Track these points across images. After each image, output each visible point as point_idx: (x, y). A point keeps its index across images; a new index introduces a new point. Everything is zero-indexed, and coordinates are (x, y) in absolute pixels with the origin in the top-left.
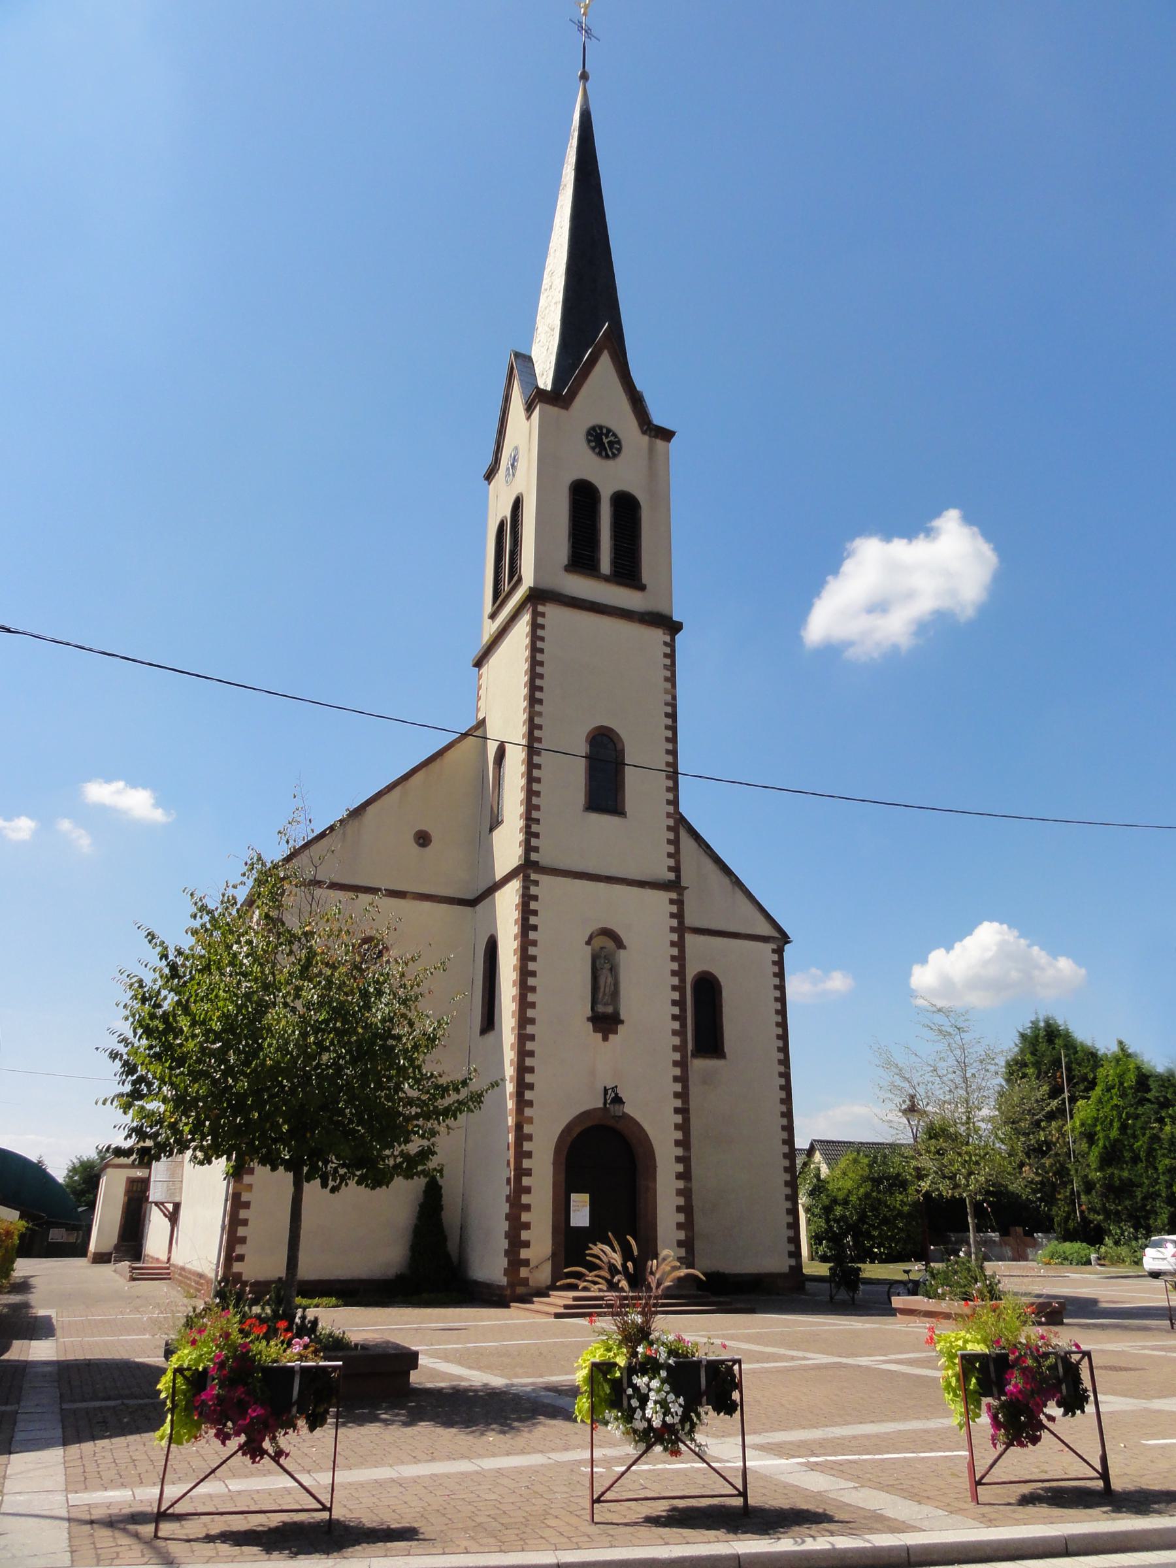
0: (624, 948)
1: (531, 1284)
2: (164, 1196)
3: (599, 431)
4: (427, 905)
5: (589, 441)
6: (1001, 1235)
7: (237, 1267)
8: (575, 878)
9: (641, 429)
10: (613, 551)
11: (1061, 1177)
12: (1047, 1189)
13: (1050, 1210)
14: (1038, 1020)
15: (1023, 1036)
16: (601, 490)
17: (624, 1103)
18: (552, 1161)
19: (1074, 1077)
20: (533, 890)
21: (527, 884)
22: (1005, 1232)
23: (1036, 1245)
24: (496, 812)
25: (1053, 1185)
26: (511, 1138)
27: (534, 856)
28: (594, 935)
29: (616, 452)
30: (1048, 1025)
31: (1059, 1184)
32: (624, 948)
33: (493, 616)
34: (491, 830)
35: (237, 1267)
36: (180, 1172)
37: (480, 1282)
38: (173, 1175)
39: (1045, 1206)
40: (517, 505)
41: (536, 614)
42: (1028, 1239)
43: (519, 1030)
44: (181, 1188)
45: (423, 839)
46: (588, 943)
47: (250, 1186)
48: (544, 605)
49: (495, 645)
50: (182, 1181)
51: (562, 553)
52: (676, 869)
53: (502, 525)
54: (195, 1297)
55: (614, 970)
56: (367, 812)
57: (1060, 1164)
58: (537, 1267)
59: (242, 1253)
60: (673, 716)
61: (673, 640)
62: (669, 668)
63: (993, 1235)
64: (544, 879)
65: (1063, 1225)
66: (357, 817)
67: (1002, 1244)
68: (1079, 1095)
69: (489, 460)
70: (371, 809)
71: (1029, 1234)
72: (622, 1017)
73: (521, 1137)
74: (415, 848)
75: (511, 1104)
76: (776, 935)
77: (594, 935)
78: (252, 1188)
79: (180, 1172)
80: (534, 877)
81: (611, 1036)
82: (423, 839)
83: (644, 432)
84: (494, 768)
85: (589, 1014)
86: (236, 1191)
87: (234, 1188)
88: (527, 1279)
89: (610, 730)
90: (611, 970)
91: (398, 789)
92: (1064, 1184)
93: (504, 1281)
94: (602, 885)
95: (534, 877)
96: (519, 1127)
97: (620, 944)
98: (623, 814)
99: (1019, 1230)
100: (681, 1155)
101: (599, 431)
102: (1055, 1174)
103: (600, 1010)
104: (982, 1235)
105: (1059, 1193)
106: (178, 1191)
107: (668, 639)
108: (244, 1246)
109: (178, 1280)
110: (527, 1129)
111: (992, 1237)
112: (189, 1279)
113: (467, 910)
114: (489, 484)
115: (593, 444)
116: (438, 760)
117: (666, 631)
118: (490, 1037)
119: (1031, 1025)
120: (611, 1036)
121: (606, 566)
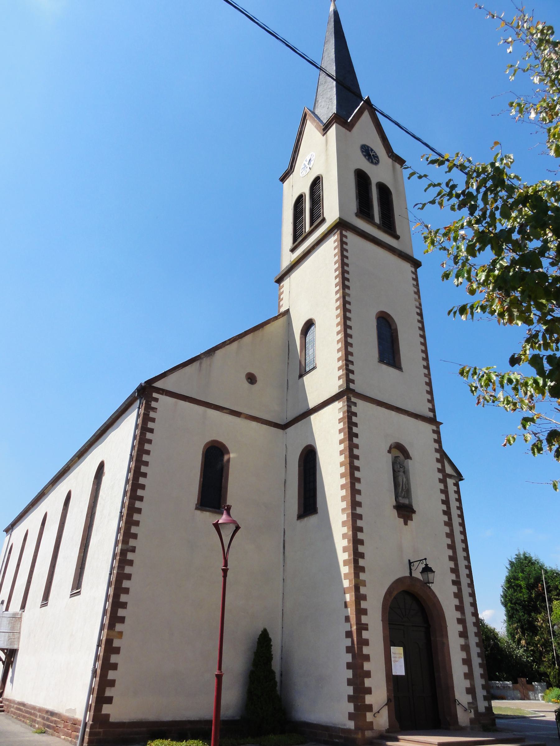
0: (411, 458)
1: (375, 728)
2: (6, 643)
3: (367, 148)
4: (254, 424)
5: (362, 152)
6: (513, 683)
7: (106, 709)
8: (378, 405)
9: (388, 155)
10: (380, 212)
11: (546, 647)
12: (537, 655)
13: (539, 667)
14: (520, 554)
15: (512, 564)
16: (372, 179)
17: (434, 572)
18: (381, 618)
19: (550, 586)
20: (354, 409)
21: (350, 404)
22: (515, 682)
23: (534, 690)
24: (304, 365)
25: (541, 653)
26: (349, 597)
27: (352, 386)
28: (392, 447)
29: (377, 162)
30: (526, 558)
31: (545, 652)
32: (411, 458)
33: (293, 250)
34: (301, 376)
35: (106, 709)
36: (19, 626)
37: (315, 724)
38: (13, 628)
39: (536, 665)
40: (317, 183)
41: (342, 236)
42: (529, 686)
43: (352, 510)
44: (19, 638)
45: (251, 379)
46: (389, 452)
47: (121, 634)
48: (346, 231)
49: (298, 264)
50: (20, 633)
51: (353, 206)
52: (433, 410)
53: (300, 200)
54: (44, 733)
55: (406, 472)
56: (215, 354)
57: (544, 639)
58: (378, 712)
59: (111, 695)
60: (421, 314)
61: (416, 271)
62: (416, 286)
63: (508, 683)
64: (359, 402)
65: (557, 677)
66: (209, 356)
67: (514, 689)
68: (554, 598)
69: (286, 167)
70: (219, 353)
71: (529, 682)
72: (415, 507)
73: (359, 598)
74: (246, 384)
75: (345, 570)
76: (454, 474)
77: (392, 447)
78: (122, 636)
79: (19, 626)
80: (353, 399)
81: (409, 522)
82: (251, 379)
83: (389, 157)
84: (301, 338)
85: (394, 503)
86: (109, 637)
87: (108, 635)
88: (372, 723)
89: (389, 315)
90: (404, 472)
91: (235, 344)
92: (548, 652)
93: (351, 725)
94: (393, 413)
95: (353, 399)
96: (357, 588)
97: (407, 456)
98: (401, 369)
99: (524, 680)
100: (460, 617)
101: (367, 148)
102: (541, 646)
103: (401, 501)
104: (501, 682)
105: (545, 657)
106: (16, 640)
107: (413, 270)
108: (113, 688)
109: (15, 713)
110: (363, 590)
111: (507, 684)
112: (34, 715)
113: (280, 431)
114: (283, 183)
115: (364, 153)
116: (261, 330)
117: (413, 266)
118: (312, 520)
119: (516, 557)
120: (409, 522)
121: (377, 219)
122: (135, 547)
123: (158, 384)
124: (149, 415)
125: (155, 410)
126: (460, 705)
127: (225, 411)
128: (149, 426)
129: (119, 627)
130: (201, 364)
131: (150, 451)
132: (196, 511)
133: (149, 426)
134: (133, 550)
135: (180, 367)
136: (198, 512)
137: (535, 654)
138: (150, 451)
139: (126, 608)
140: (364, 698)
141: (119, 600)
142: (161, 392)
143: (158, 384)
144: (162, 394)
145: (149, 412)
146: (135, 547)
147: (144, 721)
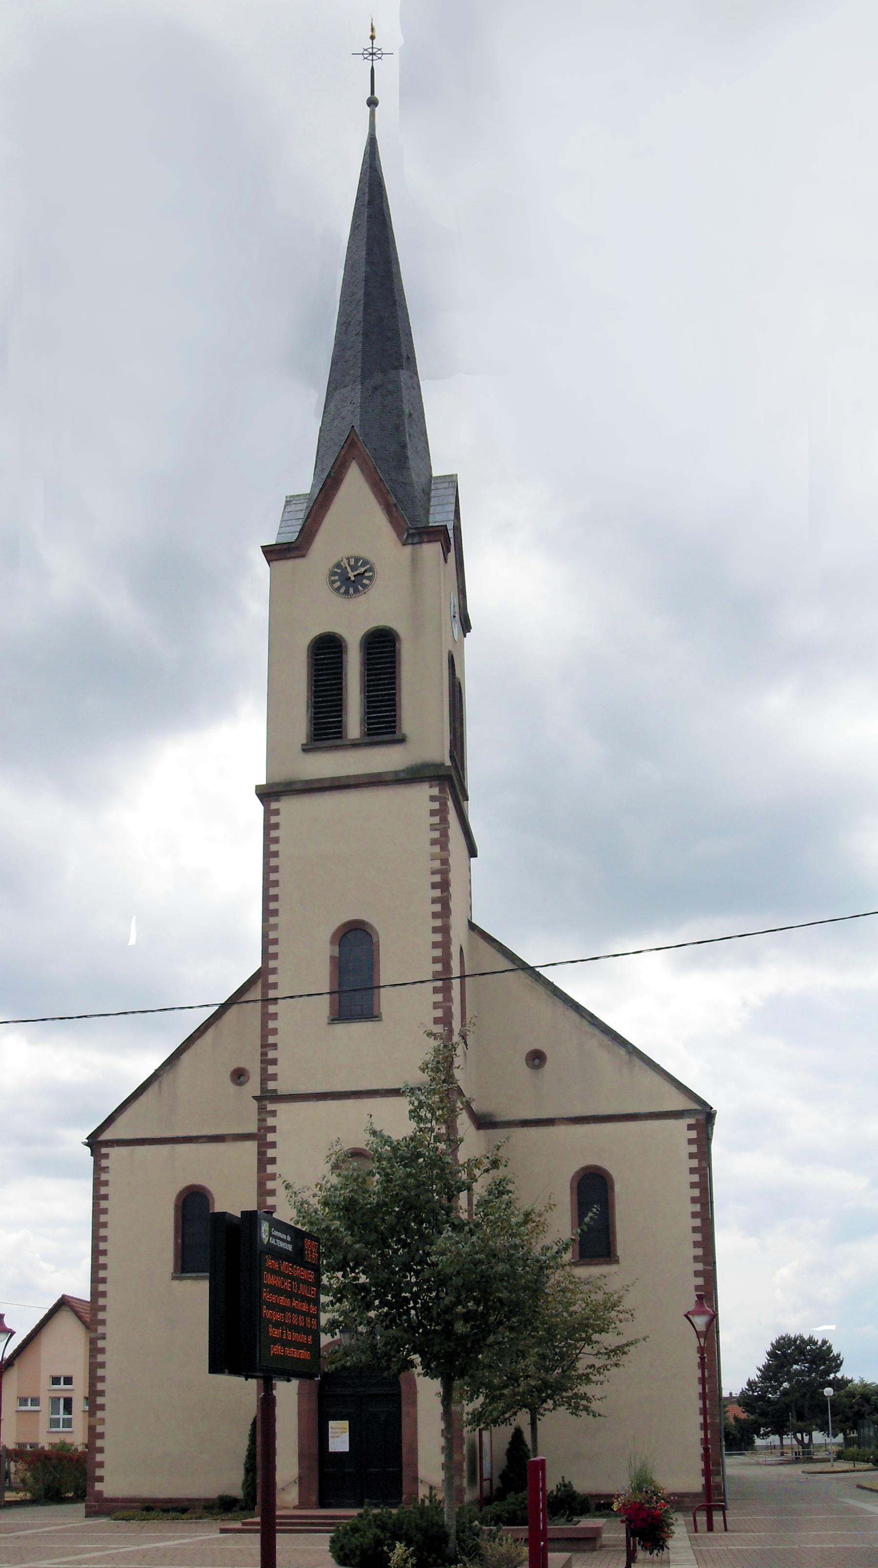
91: (211, 1032)
122: (105, 1334)
123: (106, 1136)
124: (100, 1178)
125: (106, 1170)
126: (626, 1349)
127: (200, 1140)
128: (98, 1403)
129: (100, 1414)
130: (160, 1087)
131: (103, 1448)
132: (173, 1281)
133: (98, 1403)
134: (102, 1421)
135: (132, 1099)
136: (176, 1283)
137: (850, 1431)
138: (103, 1448)
139: (104, 1396)
140: (440, 806)
141: (96, 1374)
142: (110, 1144)
143: (106, 1136)
144: (112, 1146)
145: (100, 1174)
146: (105, 1334)
147: (137, 1497)
